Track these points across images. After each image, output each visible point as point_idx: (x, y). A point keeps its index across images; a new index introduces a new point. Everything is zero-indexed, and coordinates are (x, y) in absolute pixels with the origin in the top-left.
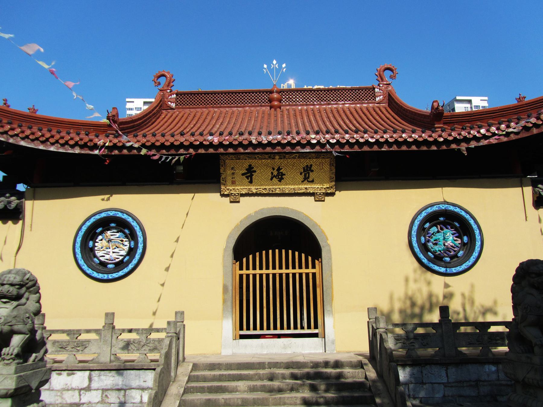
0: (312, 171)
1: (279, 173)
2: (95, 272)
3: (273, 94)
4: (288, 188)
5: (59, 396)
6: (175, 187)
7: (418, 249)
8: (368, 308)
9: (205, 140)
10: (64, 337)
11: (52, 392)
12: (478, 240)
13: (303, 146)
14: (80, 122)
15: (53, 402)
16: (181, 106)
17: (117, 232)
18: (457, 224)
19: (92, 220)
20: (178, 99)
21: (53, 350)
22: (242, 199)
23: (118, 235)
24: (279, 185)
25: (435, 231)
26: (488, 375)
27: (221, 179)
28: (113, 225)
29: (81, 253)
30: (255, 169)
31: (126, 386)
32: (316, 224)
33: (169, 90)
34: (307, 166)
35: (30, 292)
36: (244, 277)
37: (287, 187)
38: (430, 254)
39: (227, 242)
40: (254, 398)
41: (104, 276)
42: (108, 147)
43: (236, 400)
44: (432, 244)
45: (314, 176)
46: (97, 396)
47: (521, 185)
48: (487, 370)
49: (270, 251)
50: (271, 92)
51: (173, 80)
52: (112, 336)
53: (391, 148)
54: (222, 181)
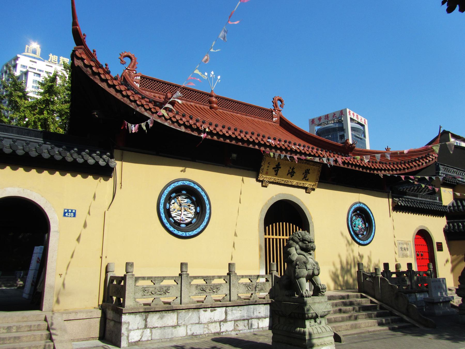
0: (309, 173)
1: (292, 171)
3: (212, 98)
4: (295, 182)
5: (206, 327)
6: (228, 169)
8: (181, 263)
10: (201, 282)
11: (201, 325)
15: (202, 333)
17: (185, 198)
18: (194, 198)
22: (270, 185)
23: (186, 201)
28: (184, 192)
31: (248, 317)
38: (171, 219)
41: (183, 234)
46: (231, 326)
49: (281, 223)
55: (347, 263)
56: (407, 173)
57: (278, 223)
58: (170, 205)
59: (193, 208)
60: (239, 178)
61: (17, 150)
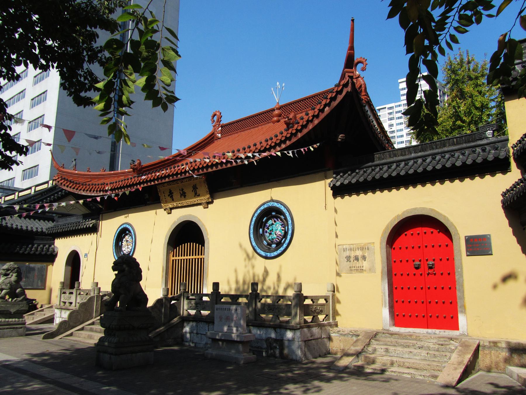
1: (183, 192)
6: (147, 207)
34: (194, 185)
39: (165, 240)
55: (244, 283)
58: (122, 242)
60: (154, 212)
61: (499, 155)
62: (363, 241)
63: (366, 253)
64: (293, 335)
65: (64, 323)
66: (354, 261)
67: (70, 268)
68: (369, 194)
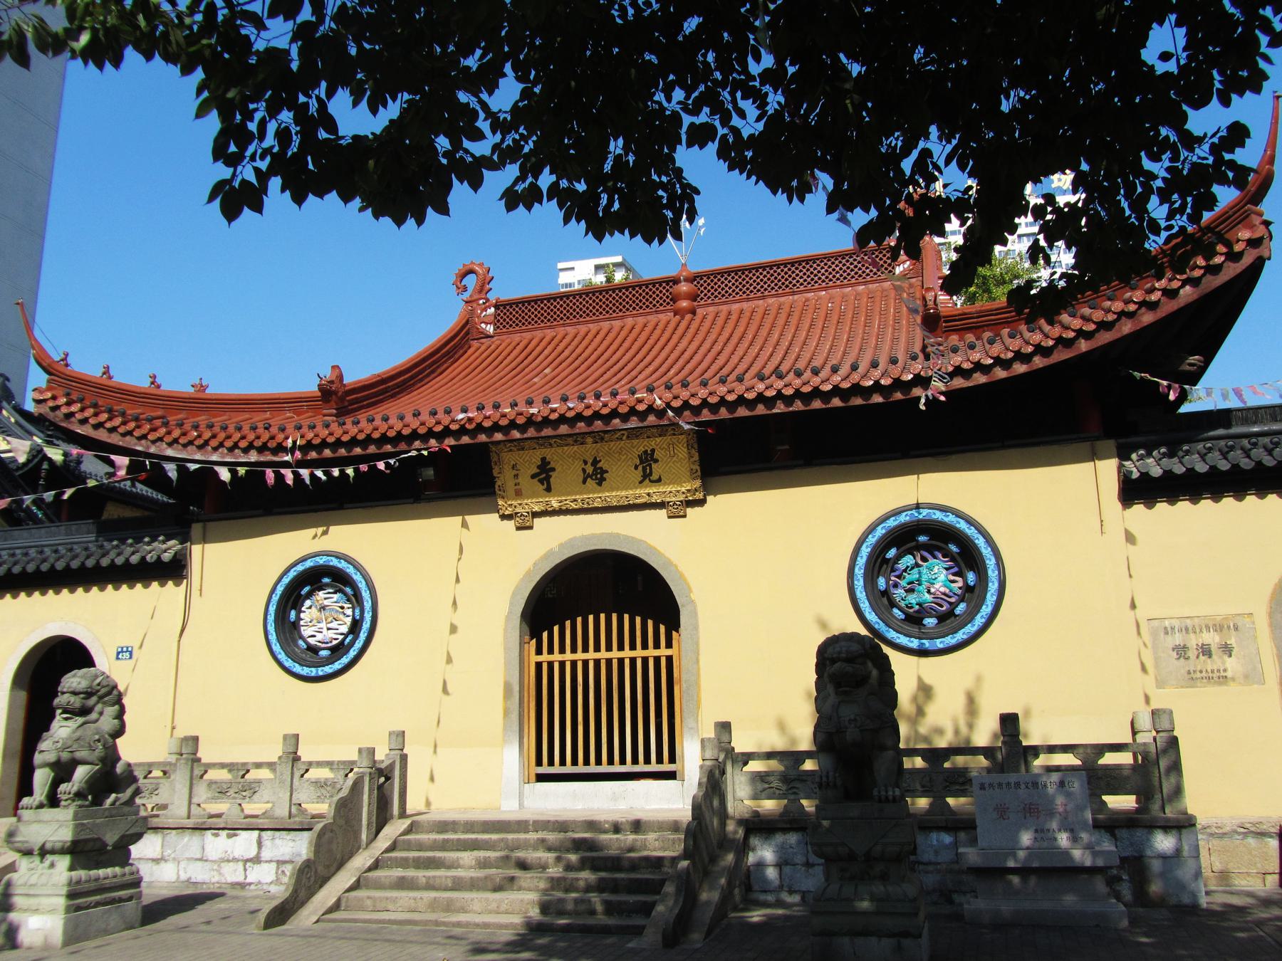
0: (656, 461)
2: (297, 665)
6: (421, 506)
7: (867, 604)
9: (453, 421)
10: (223, 775)
11: (206, 863)
12: (993, 579)
13: (625, 418)
14: (282, 397)
16: (504, 330)
17: (335, 593)
19: (292, 574)
20: (499, 315)
21: (209, 795)
23: (336, 596)
24: (599, 492)
25: (909, 564)
26: (936, 852)
27: (497, 487)
28: (326, 580)
29: (276, 631)
30: (552, 465)
32: (669, 563)
33: (481, 299)
35: (104, 703)
36: (545, 666)
37: (614, 494)
40: (471, 878)
41: (311, 671)
42: (301, 448)
43: (444, 880)
44: (903, 591)
45: (660, 471)
47: (1093, 456)
48: (935, 842)
49: (602, 616)
50: (676, 281)
51: (489, 279)
52: (292, 774)
53: (791, 406)
54: (498, 492)
56: (1086, 352)
57: (591, 618)
58: (300, 612)
59: (349, 612)
62: (1222, 609)
63: (1230, 639)
64: (1177, 844)
65: (306, 870)
66: (1198, 657)
67: (23, 695)
68: (1225, 500)
